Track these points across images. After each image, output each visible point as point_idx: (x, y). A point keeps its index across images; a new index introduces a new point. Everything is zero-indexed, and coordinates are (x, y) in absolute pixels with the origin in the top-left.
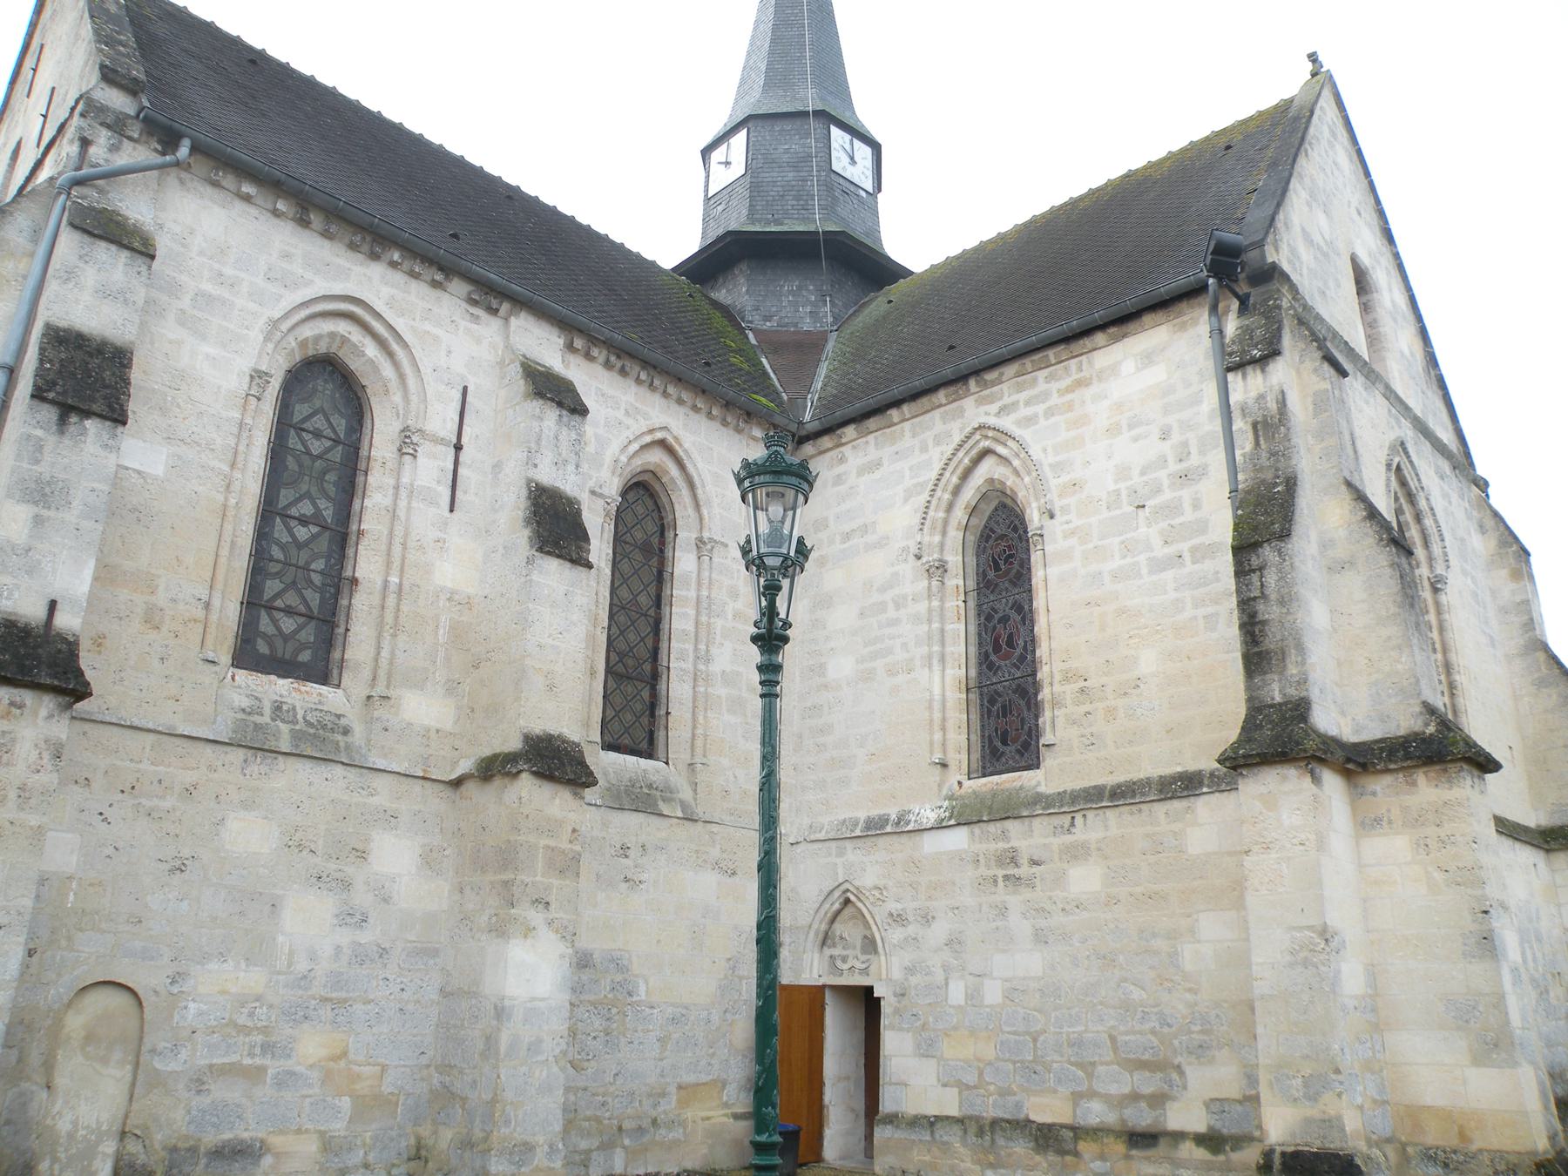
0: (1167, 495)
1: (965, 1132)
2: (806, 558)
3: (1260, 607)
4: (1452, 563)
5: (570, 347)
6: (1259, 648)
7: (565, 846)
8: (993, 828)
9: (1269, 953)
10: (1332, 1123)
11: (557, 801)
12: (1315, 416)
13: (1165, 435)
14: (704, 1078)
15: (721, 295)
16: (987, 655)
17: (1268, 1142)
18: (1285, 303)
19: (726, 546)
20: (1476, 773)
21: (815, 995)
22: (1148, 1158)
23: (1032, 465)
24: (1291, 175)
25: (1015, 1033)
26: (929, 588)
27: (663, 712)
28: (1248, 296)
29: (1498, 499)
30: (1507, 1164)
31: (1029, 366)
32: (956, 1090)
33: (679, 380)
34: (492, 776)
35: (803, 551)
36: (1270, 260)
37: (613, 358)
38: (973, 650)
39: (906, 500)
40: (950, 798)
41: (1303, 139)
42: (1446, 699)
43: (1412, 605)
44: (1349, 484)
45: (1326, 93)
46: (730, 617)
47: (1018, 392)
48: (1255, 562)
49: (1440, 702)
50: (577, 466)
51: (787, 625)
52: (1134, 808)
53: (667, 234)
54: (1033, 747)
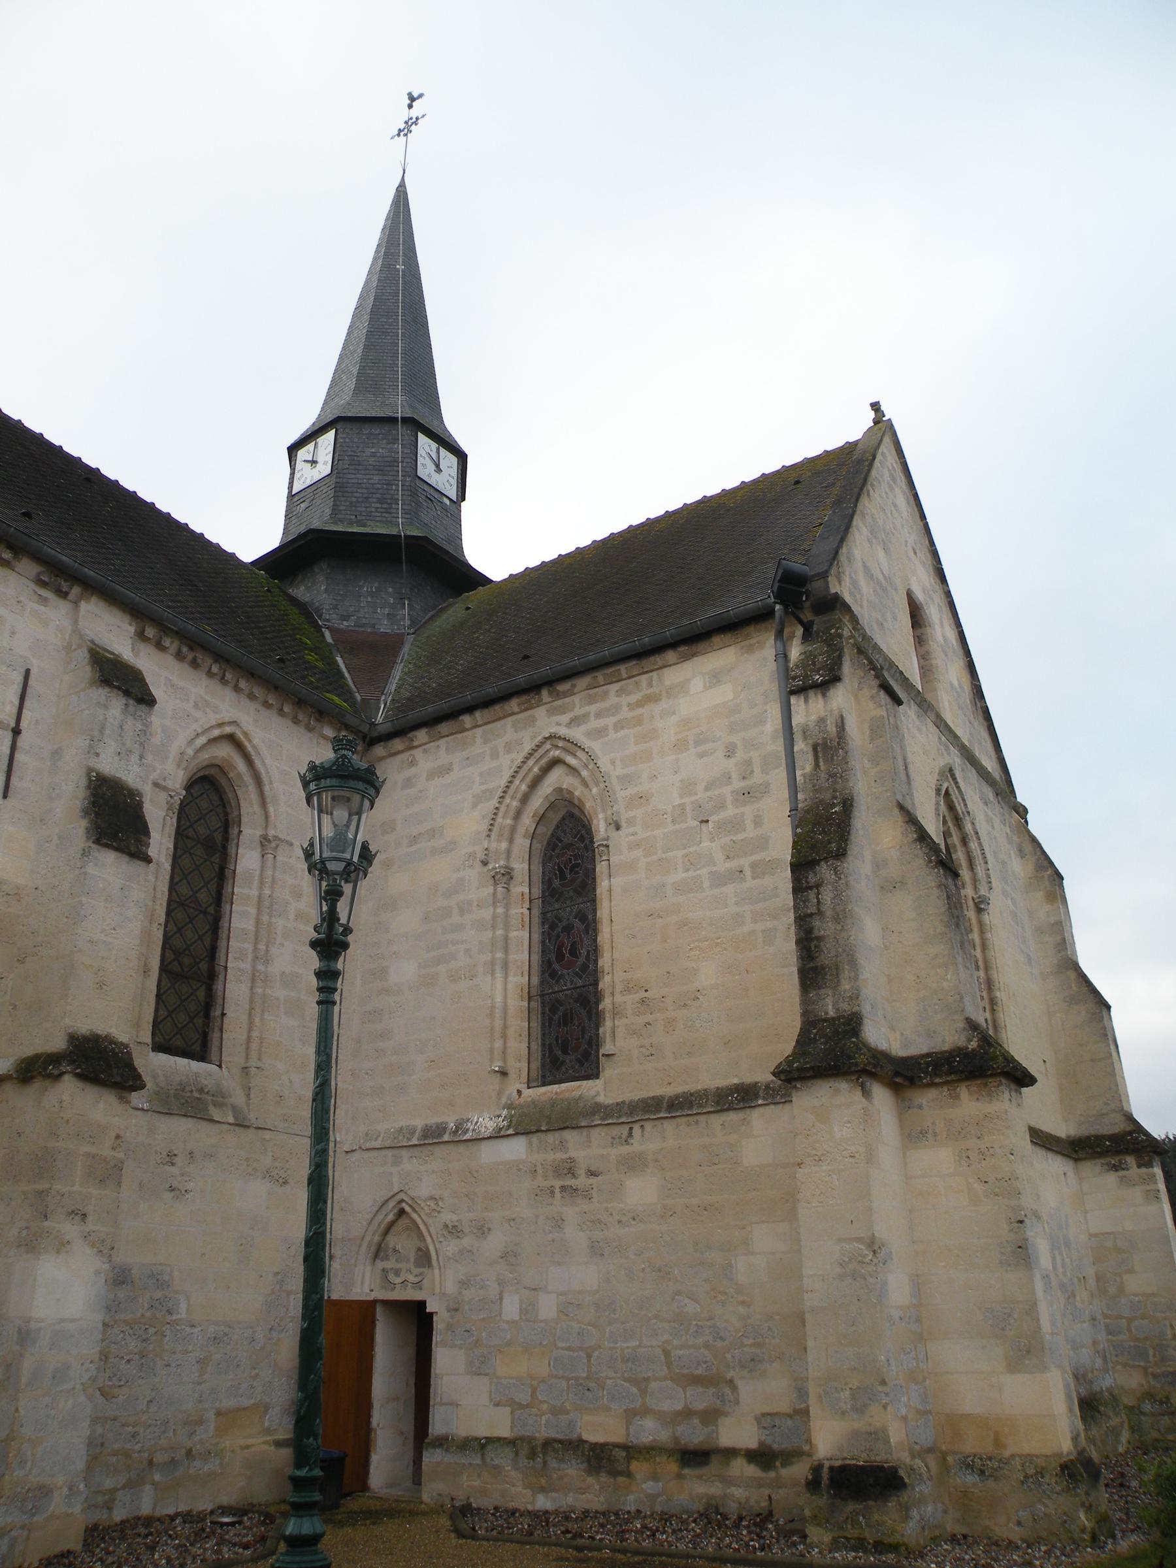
0: (731, 811)
1: (517, 1454)
2: (370, 863)
3: (816, 923)
4: (994, 884)
5: (141, 635)
6: (815, 964)
7: (106, 1152)
8: (551, 1138)
9: (820, 1263)
10: (878, 1435)
11: (101, 1105)
12: (872, 740)
13: (730, 753)
14: (246, 1402)
15: (300, 592)
16: (549, 963)
17: (815, 1458)
18: (846, 633)
19: (291, 844)
20: (1013, 1086)
21: (365, 1310)
22: (700, 1477)
23: (599, 776)
24: (854, 512)
25: (569, 1349)
26: (495, 894)
27: (218, 1013)
28: (811, 623)
29: (1035, 826)
30: (1036, 1467)
31: (601, 679)
32: (508, 1410)
33: (251, 675)
34: (32, 1078)
35: (367, 855)
36: (833, 591)
37: (185, 650)
38: (536, 958)
39: (474, 806)
40: (509, 1107)
41: (865, 481)
42: (988, 1015)
43: (957, 925)
44: (901, 807)
45: (887, 440)
46: (292, 917)
47: (590, 704)
48: (812, 879)
49: (981, 1018)
50: (141, 757)
51: (347, 930)
52: (691, 1119)
53: (249, 528)
54: (592, 1057)
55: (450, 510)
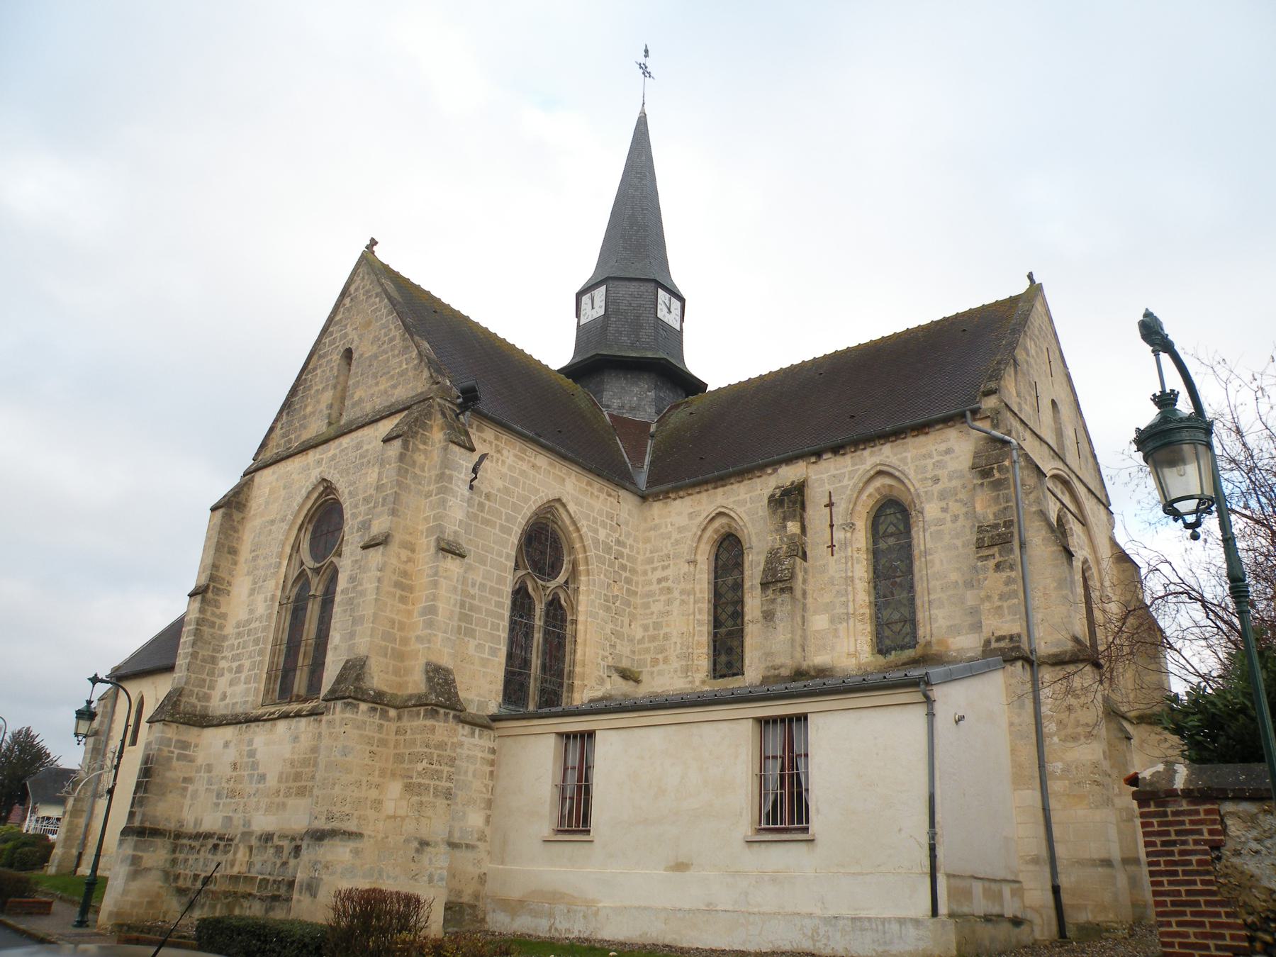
53: (551, 343)
55: (675, 338)
